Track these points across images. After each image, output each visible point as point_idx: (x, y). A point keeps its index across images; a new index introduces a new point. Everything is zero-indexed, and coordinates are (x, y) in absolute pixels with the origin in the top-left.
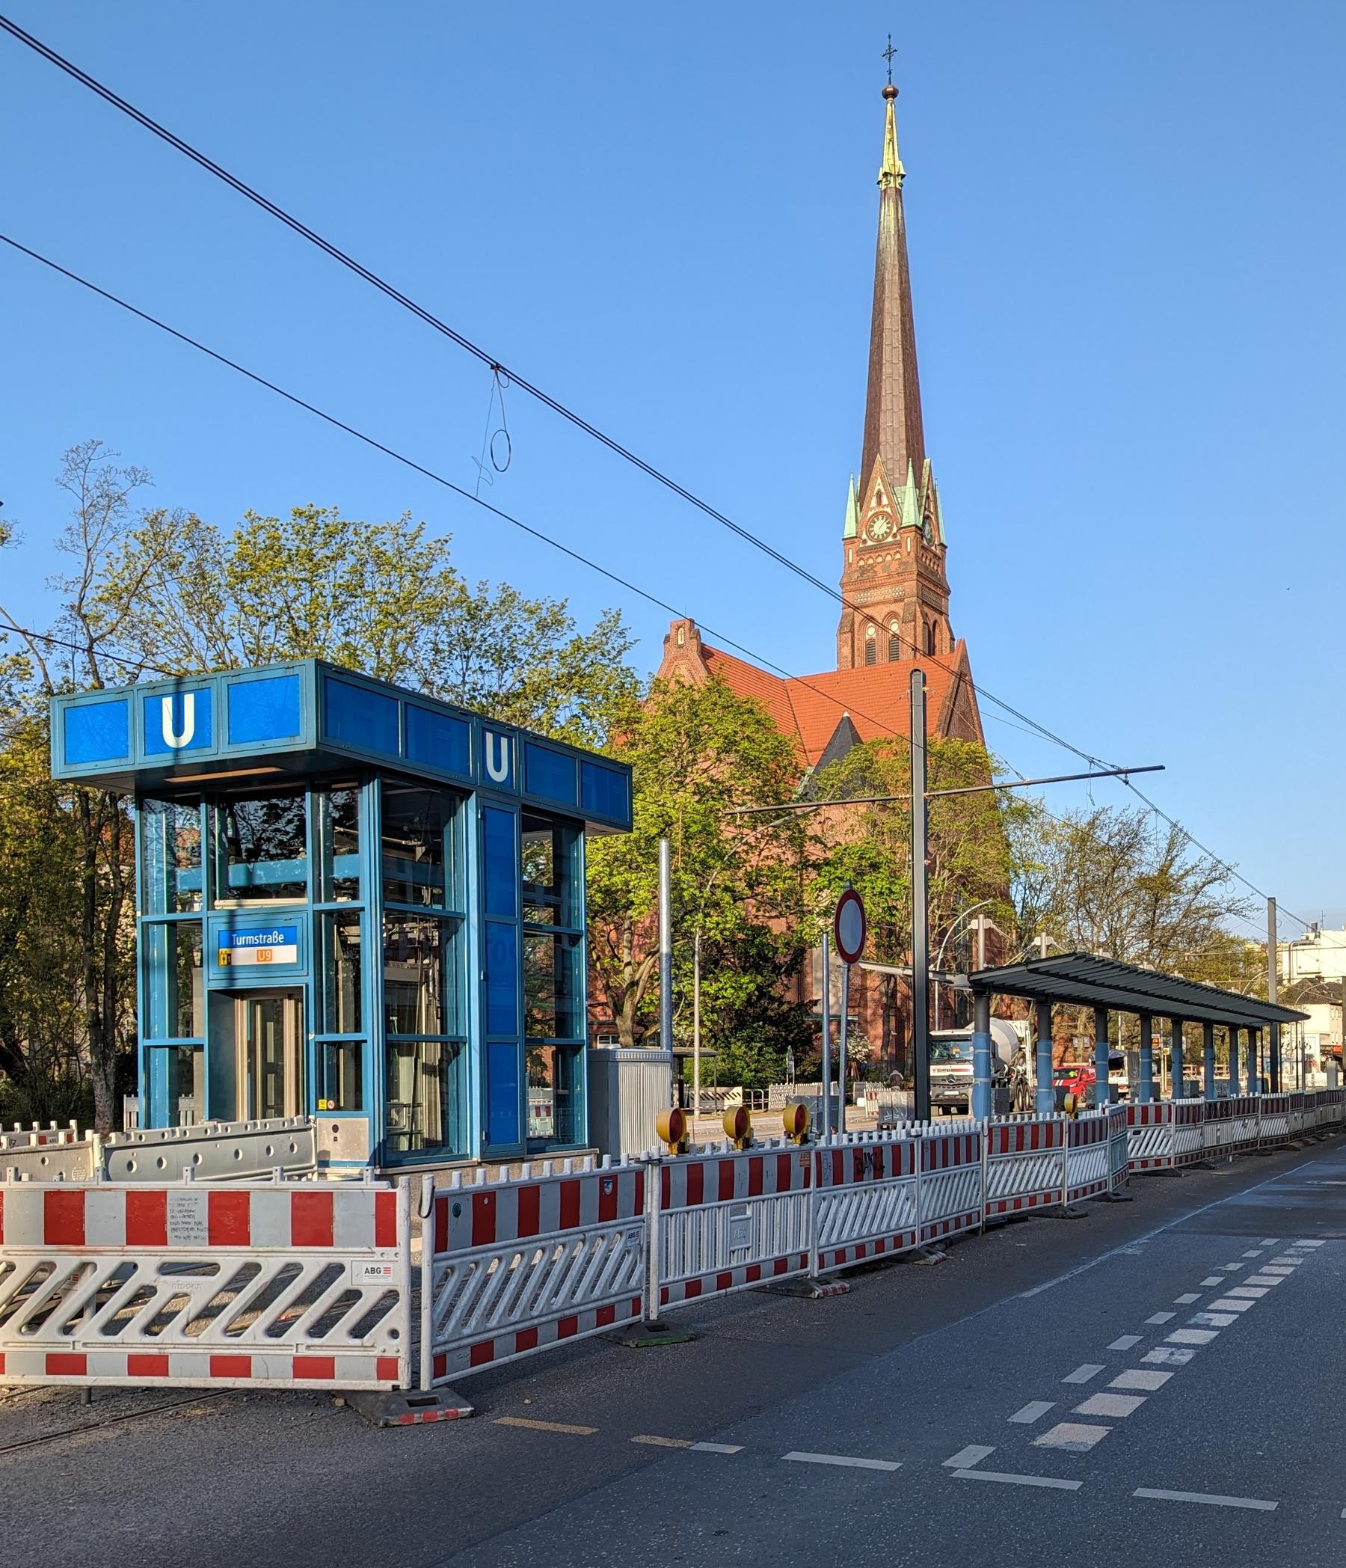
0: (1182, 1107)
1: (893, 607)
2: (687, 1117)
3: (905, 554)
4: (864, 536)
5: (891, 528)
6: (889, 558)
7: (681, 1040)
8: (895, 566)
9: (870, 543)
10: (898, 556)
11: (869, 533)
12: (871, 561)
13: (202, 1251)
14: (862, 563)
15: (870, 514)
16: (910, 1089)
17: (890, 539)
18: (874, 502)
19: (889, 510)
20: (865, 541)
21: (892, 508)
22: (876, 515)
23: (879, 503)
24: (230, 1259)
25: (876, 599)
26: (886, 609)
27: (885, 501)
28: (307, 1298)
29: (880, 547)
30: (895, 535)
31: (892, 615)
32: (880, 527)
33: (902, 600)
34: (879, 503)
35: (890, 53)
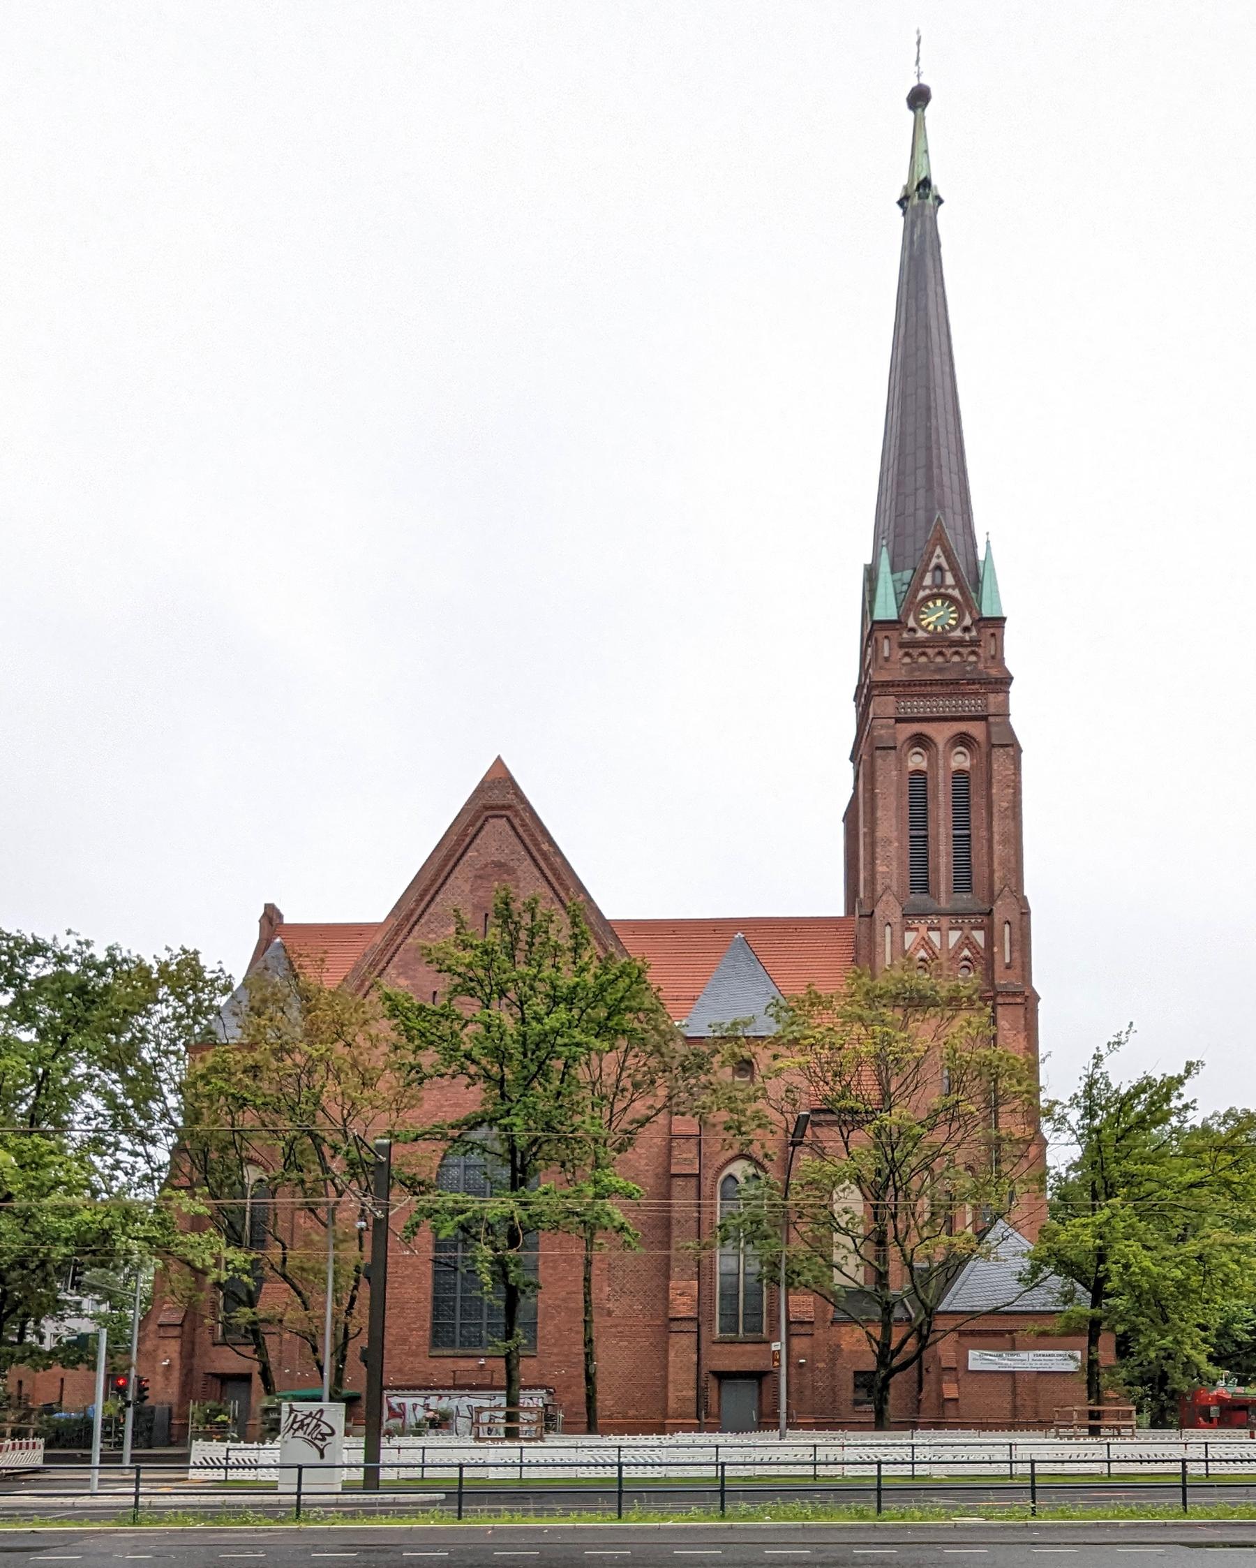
9: (921, 634)
11: (918, 621)
15: (922, 594)
17: (958, 633)
19: (956, 593)
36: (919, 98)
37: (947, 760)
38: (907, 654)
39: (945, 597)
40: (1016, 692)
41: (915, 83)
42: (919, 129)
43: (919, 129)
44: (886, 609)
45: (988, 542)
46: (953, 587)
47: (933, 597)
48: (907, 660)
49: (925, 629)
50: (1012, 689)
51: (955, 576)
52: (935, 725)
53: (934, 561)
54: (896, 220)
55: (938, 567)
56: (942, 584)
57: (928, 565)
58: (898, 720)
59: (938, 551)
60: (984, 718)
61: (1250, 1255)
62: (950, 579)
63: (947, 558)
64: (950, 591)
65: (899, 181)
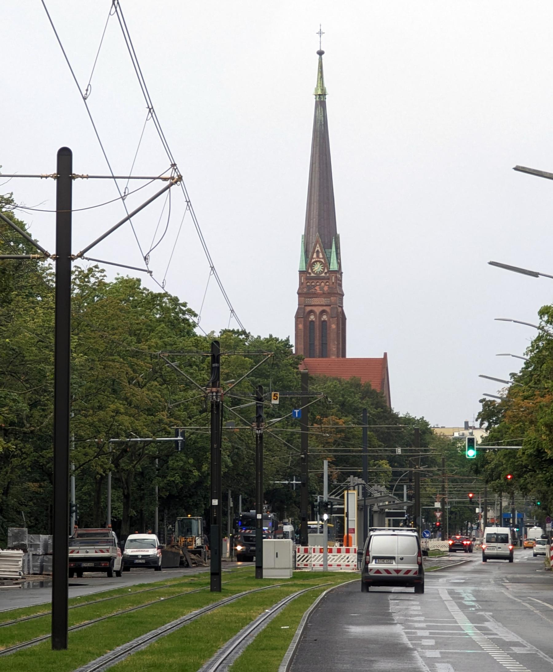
0: (314, 520)
1: (324, 308)
2: (497, 568)
3: (331, 283)
4: (310, 271)
5: (324, 269)
6: (323, 284)
7: (119, 465)
8: (326, 288)
9: (312, 275)
10: (327, 284)
11: (312, 270)
12: (313, 284)
13: (336, 554)
14: (308, 284)
15: (313, 261)
16: (49, 587)
17: (323, 275)
18: (315, 256)
19: (323, 260)
20: (310, 273)
21: (325, 260)
22: (316, 261)
23: (318, 256)
24: (339, 555)
25: (316, 303)
26: (321, 308)
27: (321, 256)
28: (316, 559)
29: (318, 278)
30: (326, 273)
31: (323, 312)
32: (318, 268)
33: (330, 305)
34: (318, 256)
35: (320, 33)
36: (321, 53)
41: (319, 49)
46: (322, 258)
51: (323, 255)
52: (317, 307)
55: (318, 251)
57: (314, 250)
58: (306, 306)
59: (318, 245)
62: (321, 256)
64: (321, 260)
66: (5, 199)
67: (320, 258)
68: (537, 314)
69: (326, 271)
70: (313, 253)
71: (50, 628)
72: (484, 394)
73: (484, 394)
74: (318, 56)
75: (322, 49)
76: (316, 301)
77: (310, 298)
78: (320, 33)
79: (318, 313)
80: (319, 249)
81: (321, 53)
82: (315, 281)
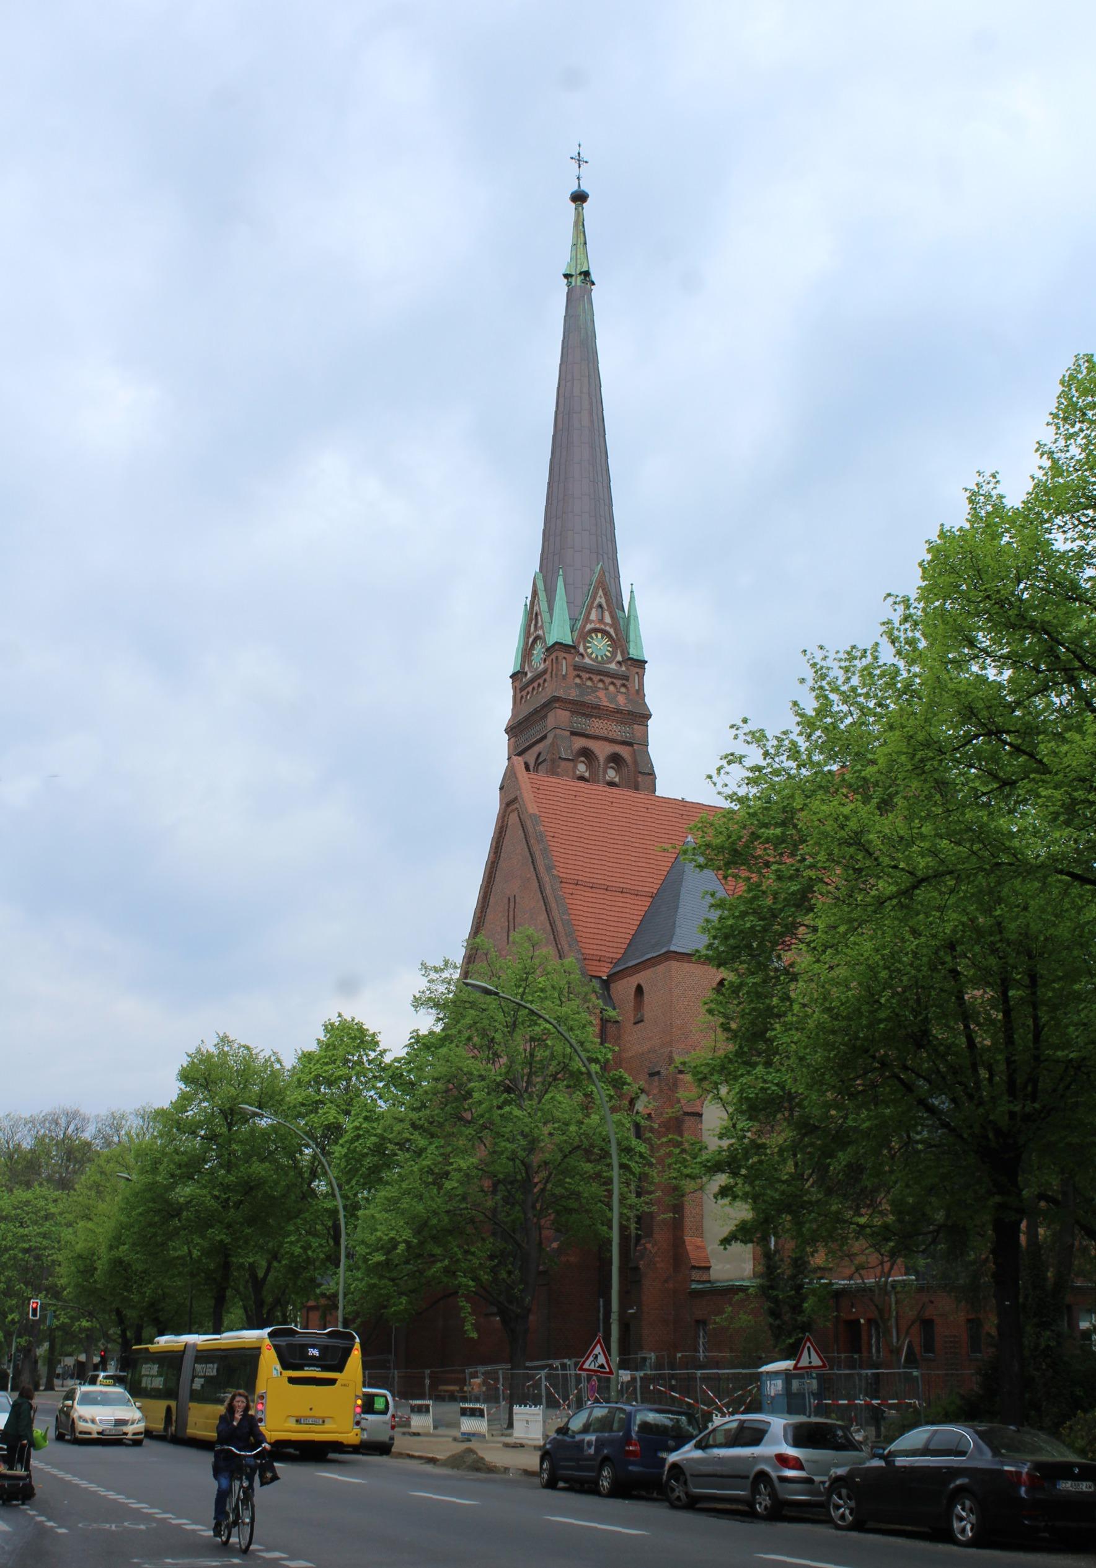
5: (614, 654)
11: (586, 648)
15: (589, 627)
22: (596, 630)
25: (597, 733)
36: (579, 198)
37: (605, 772)
38: (579, 676)
39: (605, 633)
40: (655, 728)
41: (575, 188)
42: (579, 224)
43: (579, 224)
44: (559, 631)
45: (632, 592)
47: (596, 630)
48: (578, 681)
49: (590, 656)
50: (649, 722)
51: (612, 617)
52: (601, 743)
53: (598, 600)
54: (561, 289)
55: (600, 606)
56: (601, 621)
57: (593, 603)
58: (573, 733)
59: (600, 593)
60: (630, 744)
61: (1092, 789)
63: (607, 601)
64: (608, 628)
65: (562, 261)
66: (875, 1190)
67: (606, 624)
68: (1063, 366)
69: (619, 658)
70: (590, 608)
71: (9, 1409)
72: (332, 1382)
73: (332, 1382)
74: (573, 205)
75: (583, 188)
76: (598, 726)
77: (584, 715)
78: (579, 160)
79: (602, 759)
80: (603, 601)
81: (579, 198)
82: (596, 678)
